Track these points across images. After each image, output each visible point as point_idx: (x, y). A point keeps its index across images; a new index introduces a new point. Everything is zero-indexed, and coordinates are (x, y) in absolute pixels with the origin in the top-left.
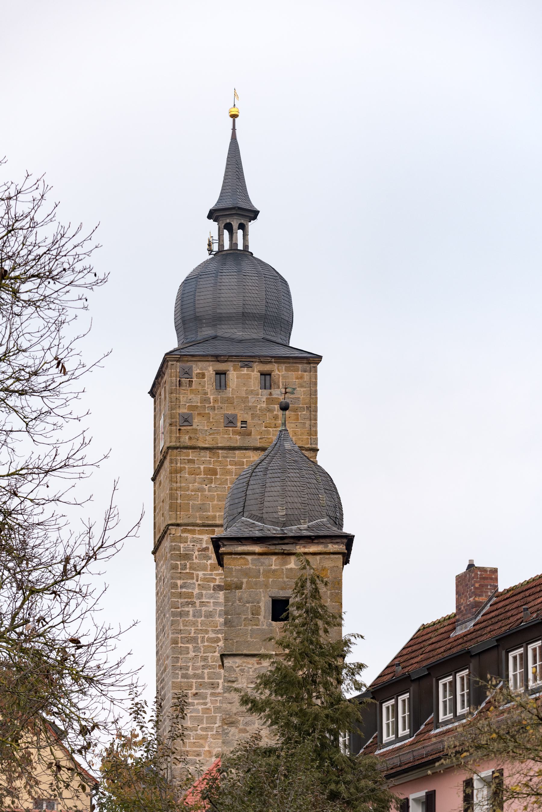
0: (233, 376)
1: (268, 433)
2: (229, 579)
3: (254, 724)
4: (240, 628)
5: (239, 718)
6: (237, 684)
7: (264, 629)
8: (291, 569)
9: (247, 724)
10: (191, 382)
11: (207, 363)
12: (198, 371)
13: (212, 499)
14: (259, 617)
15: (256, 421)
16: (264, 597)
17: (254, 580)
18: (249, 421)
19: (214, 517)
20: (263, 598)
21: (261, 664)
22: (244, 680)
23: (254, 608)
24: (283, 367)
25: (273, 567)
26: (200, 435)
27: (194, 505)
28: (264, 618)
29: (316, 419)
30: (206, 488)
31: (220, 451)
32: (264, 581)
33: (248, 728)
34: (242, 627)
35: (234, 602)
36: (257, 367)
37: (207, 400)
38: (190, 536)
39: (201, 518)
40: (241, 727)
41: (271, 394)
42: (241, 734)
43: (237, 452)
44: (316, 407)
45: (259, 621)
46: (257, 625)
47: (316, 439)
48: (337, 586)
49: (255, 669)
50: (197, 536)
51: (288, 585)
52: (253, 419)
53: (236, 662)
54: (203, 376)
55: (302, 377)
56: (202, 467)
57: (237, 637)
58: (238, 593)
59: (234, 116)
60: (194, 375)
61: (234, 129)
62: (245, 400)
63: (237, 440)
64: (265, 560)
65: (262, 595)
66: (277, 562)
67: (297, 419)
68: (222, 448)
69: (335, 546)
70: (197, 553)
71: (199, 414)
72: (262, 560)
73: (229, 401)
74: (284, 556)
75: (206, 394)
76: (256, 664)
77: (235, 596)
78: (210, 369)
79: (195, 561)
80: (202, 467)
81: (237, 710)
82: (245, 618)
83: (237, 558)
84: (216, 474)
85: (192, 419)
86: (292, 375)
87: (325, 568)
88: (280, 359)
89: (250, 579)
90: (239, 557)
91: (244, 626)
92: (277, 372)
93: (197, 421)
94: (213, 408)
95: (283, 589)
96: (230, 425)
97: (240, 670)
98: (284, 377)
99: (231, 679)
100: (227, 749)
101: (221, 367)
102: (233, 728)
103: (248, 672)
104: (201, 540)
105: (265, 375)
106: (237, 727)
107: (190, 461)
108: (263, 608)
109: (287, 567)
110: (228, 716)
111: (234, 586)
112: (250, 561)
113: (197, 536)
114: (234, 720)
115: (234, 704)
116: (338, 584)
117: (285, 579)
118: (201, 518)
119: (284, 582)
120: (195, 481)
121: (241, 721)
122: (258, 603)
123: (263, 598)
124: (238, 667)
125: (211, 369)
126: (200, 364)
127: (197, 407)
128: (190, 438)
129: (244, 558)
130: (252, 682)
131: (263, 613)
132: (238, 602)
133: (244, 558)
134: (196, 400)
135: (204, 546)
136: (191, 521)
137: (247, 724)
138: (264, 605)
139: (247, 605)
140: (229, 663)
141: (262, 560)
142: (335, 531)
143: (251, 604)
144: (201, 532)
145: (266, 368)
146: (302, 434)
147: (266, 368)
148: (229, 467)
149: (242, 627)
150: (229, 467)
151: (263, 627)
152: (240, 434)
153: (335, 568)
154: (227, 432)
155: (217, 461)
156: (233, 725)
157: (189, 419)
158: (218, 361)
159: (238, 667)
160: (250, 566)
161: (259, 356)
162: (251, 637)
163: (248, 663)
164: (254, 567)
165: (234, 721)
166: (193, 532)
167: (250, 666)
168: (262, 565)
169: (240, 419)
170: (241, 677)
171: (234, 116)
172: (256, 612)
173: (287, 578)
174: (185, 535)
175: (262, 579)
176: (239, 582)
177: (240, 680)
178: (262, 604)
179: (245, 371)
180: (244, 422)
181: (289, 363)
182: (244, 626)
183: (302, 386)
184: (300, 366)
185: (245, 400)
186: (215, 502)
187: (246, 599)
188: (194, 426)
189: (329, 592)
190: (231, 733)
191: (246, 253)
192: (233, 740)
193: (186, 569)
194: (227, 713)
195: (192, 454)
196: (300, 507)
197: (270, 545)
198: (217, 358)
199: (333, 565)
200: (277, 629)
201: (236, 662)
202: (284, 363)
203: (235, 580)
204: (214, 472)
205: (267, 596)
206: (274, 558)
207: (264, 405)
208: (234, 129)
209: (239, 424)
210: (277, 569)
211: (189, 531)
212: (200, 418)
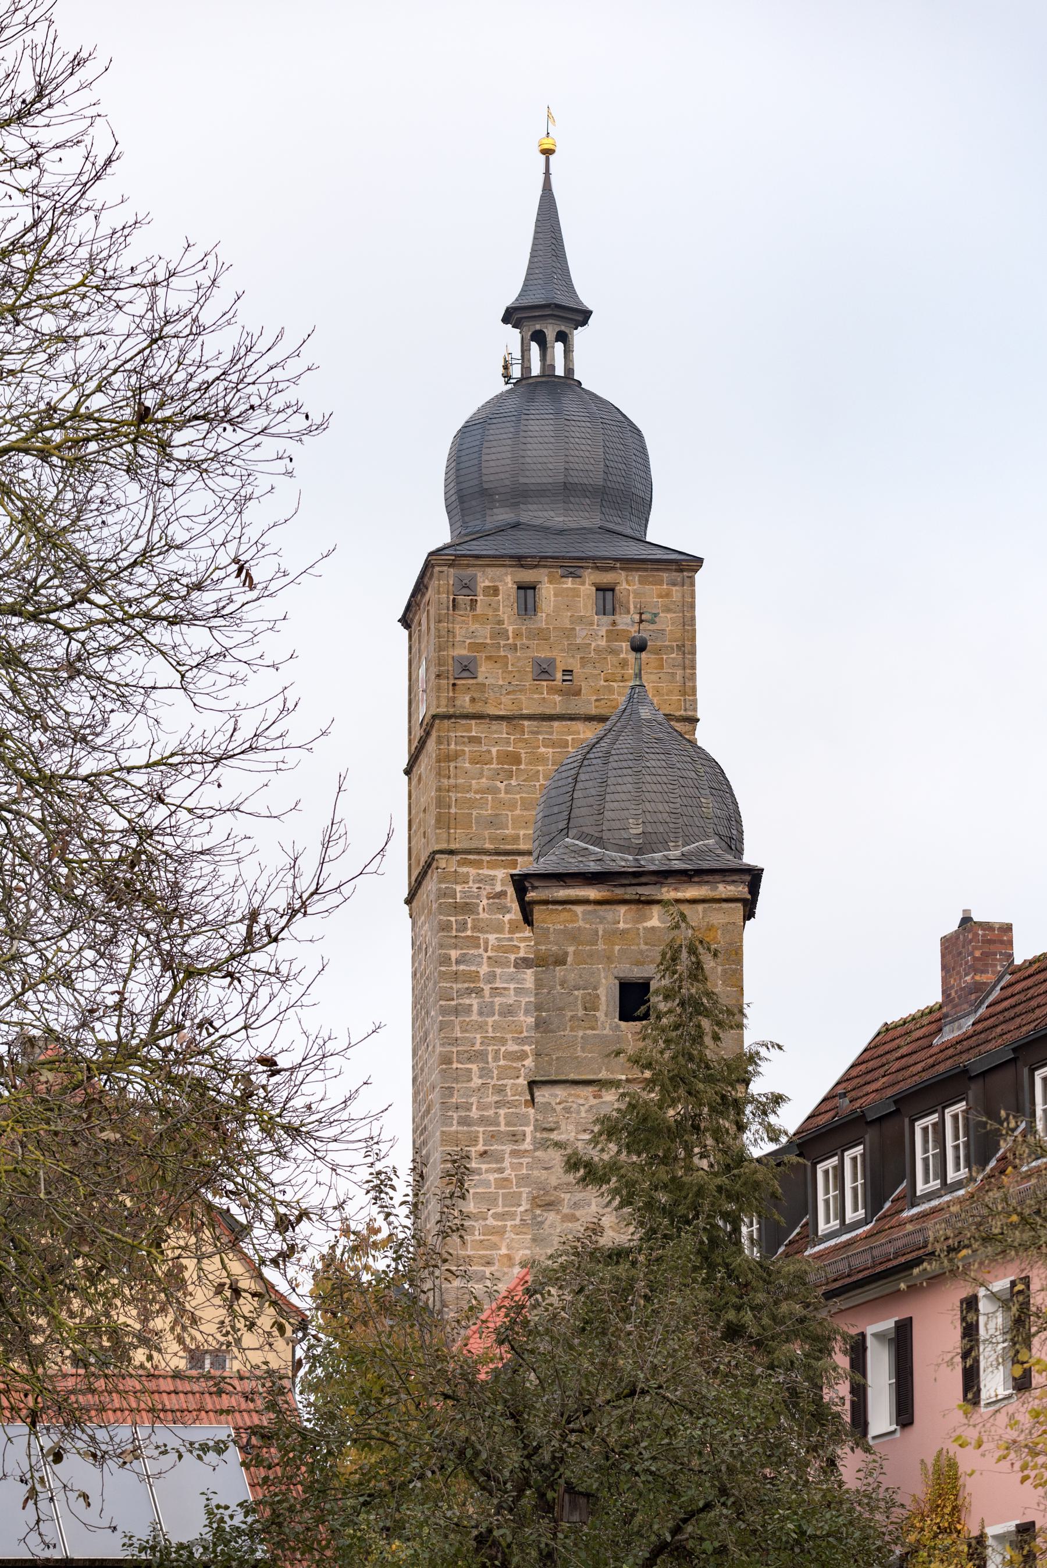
0: (548, 592)
2: (544, 948)
3: (589, 1205)
5: (562, 1195)
6: (559, 1134)
7: (606, 1036)
8: (653, 928)
9: (576, 1205)
10: (474, 602)
11: (503, 570)
12: (487, 583)
13: (512, 806)
15: (588, 670)
16: (606, 978)
17: (588, 948)
18: (577, 669)
19: (516, 839)
20: (603, 981)
21: (600, 1097)
22: (571, 1127)
23: (588, 998)
24: (636, 576)
25: (621, 925)
26: (490, 695)
27: (480, 816)
28: (606, 1016)
30: (502, 786)
31: (526, 723)
33: (578, 1213)
34: (566, 1033)
36: (591, 577)
38: (472, 871)
39: (492, 840)
40: (566, 1210)
41: (614, 623)
42: (565, 1225)
43: (556, 724)
44: (694, 646)
46: (593, 1029)
47: (695, 701)
50: (486, 872)
51: (647, 956)
52: (583, 666)
53: (557, 1095)
54: (496, 591)
55: (668, 595)
56: (494, 750)
59: (547, 152)
60: (479, 590)
61: (547, 173)
62: (570, 633)
63: (557, 704)
64: (608, 913)
65: (602, 975)
67: (661, 667)
69: (729, 888)
70: (485, 902)
71: (489, 658)
73: (541, 635)
75: (500, 622)
76: (591, 1098)
77: (554, 977)
78: (507, 580)
79: (483, 915)
80: (494, 750)
84: (519, 763)
85: (476, 666)
88: (630, 564)
90: (560, 908)
93: (485, 671)
95: (638, 963)
96: (545, 676)
98: (637, 594)
100: (541, 1252)
103: (579, 1112)
104: (493, 878)
106: (558, 1212)
108: (603, 999)
109: (645, 924)
110: (542, 1192)
111: (551, 960)
113: (486, 872)
114: (552, 1198)
116: (737, 954)
117: (643, 947)
118: (492, 840)
119: (641, 952)
120: (481, 775)
122: (595, 988)
123: (603, 981)
124: (560, 1103)
125: (509, 579)
126: (490, 571)
127: (484, 645)
128: (473, 700)
129: (570, 910)
130: (585, 1131)
131: (603, 1007)
132: (559, 987)
133: (570, 910)
134: (484, 633)
136: (474, 844)
137: (576, 1205)
139: (576, 993)
140: (544, 1096)
144: (492, 865)
146: (670, 692)
147: (607, 578)
148: (542, 750)
149: (566, 1033)
150: (542, 750)
151: (605, 1032)
152: (560, 692)
154: (537, 690)
155: (521, 740)
156: (551, 1208)
157: (471, 667)
158: (522, 566)
159: (560, 1103)
160: (581, 923)
161: (594, 558)
162: (583, 1049)
163: (578, 1096)
164: (588, 926)
166: (478, 864)
167: (581, 1101)
168: (601, 923)
170: (565, 1121)
171: (547, 152)
172: (590, 1005)
173: (646, 944)
174: (464, 870)
175: (601, 946)
177: (563, 1127)
178: (602, 992)
179: (569, 583)
180: (568, 672)
181: (646, 570)
183: (668, 610)
184: (665, 575)
185: (570, 633)
186: (518, 812)
187: (573, 983)
188: (480, 679)
189: (720, 968)
190: (548, 1222)
193: (465, 929)
195: (475, 729)
197: (615, 886)
198: (520, 561)
200: (630, 1036)
201: (557, 1095)
202: (638, 570)
204: (516, 759)
205: (611, 977)
207: (603, 643)
208: (547, 173)
209: (559, 676)
210: (628, 929)
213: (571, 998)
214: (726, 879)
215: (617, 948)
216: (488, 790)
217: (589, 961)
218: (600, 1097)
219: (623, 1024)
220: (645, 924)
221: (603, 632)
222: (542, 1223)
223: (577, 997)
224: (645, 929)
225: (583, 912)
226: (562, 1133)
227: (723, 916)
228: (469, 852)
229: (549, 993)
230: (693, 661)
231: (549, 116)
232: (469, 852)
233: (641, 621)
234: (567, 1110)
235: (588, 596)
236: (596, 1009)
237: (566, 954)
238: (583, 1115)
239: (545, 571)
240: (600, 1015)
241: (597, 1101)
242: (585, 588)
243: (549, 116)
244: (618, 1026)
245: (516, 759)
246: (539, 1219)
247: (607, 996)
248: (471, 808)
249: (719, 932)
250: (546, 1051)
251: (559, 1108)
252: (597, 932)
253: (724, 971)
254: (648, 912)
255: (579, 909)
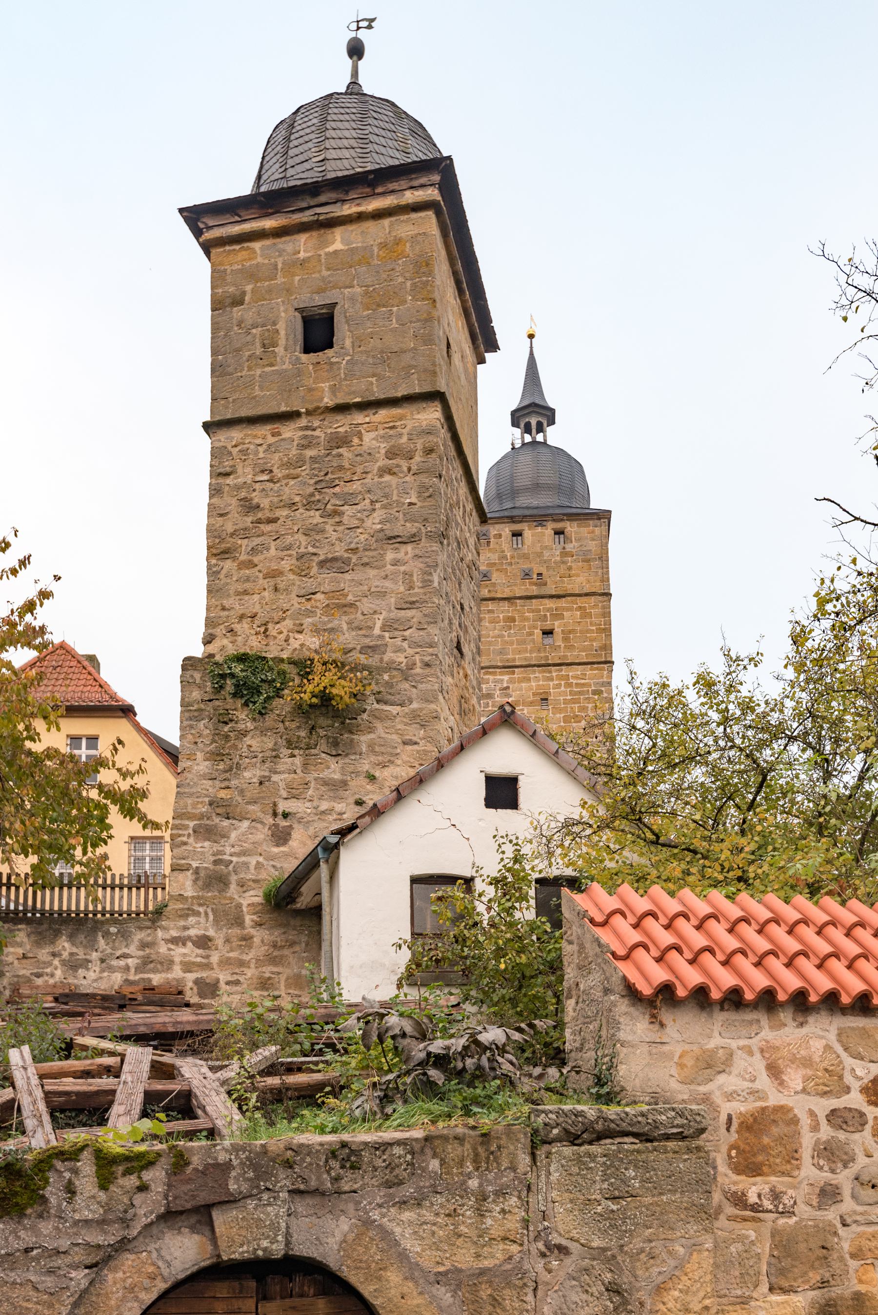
0: (528, 534)
1: (563, 582)
2: (220, 291)
3: (268, 549)
4: (239, 374)
5: (239, 542)
6: (236, 478)
7: (286, 371)
8: (336, 252)
9: (254, 551)
10: (489, 543)
11: (504, 525)
12: (496, 532)
13: (512, 643)
14: (276, 350)
15: (551, 572)
16: (285, 311)
17: (267, 283)
18: (544, 572)
19: (514, 660)
20: (283, 314)
21: (279, 434)
22: (248, 470)
23: (267, 334)
24: (575, 524)
25: (302, 255)
26: (498, 588)
27: (494, 649)
28: (286, 350)
29: (608, 568)
30: (506, 634)
31: (518, 601)
32: (284, 283)
33: (256, 560)
34: (244, 373)
35: (229, 330)
36: (551, 526)
37: (505, 557)
38: (491, 677)
39: (501, 661)
40: (243, 557)
41: (564, 548)
42: (242, 572)
43: (534, 601)
44: (608, 557)
45: (275, 357)
46: (272, 365)
47: (609, 585)
48: (424, 269)
49: (270, 445)
50: (498, 677)
51: (330, 282)
52: (548, 571)
53: (233, 438)
54: (500, 536)
55: (593, 532)
56: (501, 616)
57: (235, 391)
58: (237, 312)
59: (531, 336)
60: (492, 536)
61: (531, 347)
62: (540, 555)
63: (534, 590)
64: (287, 244)
65: (282, 309)
66: (309, 245)
67: (590, 569)
68: (520, 598)
69: (416, 193)
70: (498, 692)
71: (497, 570)
72: (281, 246)
73: (526, 557)
74: (322, 231)
75: (503, 551)
76: (269, 436)
77: (231, 318)
78: (506, 530)
79: (497, 699)
80: (501, 616)
81: (235, 527)
82: (250, 356)
83: (234, 250)
84: (515, 621)
85: (491, 574)
86: (584, 531)
87: (400, 239)
88: (572, 517)
89: (259, 284)
90: (237, 247)
91: (248, 370)
92: (569, 529)
93: (496, 577)
94: (511, 564)
95: (320, 291)
96: (527, 577)
97: (240, 451)
98: (576, 533)
99: (222, 470)
100: (216, 603)
101: (517, 527)
102: (229, 562)
103: (256, 453)
104: (502, 680)
105: (559, 532)
106: (234, 559)
107: (490, 611)
108: (282, 333)
109: (327, 250)
110: (217, 541)
111: (228, 301)
112: (258, 252)
113: (498, 677)
114: (228, 545)
115: (229, 516)
116: (427, 265)
117: (325, 273)
118: (501, 661)
119: (323, 279)
120: (495, 629)
121: (244, 547)
122: (274, 323)
123: (283, 314)
124: (236, 446)
125: (507, 530)
126: (497, 526)
127: (495, 564)
128: (489, 591)
129: (248, 248)
130: (263, 471)
131: (282, 342)
132: (236, 328)
133: (248, 248)
134: (494, 557)
135: (505, 685)
136: (493, 663)
137: (254, 551)
138: (284, 326)
139: (254, 331)
140: (220, 441)
141: (281, 246)
142: (418, 154)
143: (260, 329)
144: (501, 674)
145: (559, 525)
146: (595, 581)
147: (559, 525)
148: (527, 614)
149: (244, 373)
150: (527, 614)
151: (284, 367)
152: (536, 584)
153: (420, 238)
154: (524, 584)
155: (516, 610)
156: (227, 556)
157: (488, 575)
158: (514, 522)
159: (236, 446)
160: (259, 259)
161: (551, 515)
162: (261, 388)
163: (255, 436)
164: (266, 261)
165: (229, 548)
166: (494, 674)
167: (259, 441)
168: (280, 256)
169: (536, 571)
170: (241, 464)
171: (531, 336)
172: (269, 344)
173: (328, 269)
174: (487, 677)
175: (280, 280)
176: (238, 293)
177: (240, 470)
178: (281, 326)
179: (539, 529)
180: (540, 574)
181: (580, 520)
182: (248, 370)
183: (593, 540)
184: (591, 522)
185: (540, 555)
186: (515, 646)
187: (250, 321)
188: (493, 581)
189: (409, 283)
190: (224, 572)
191: (545, 443)
192: (227, 584)
193: (488, 707)
194: (216, 534)
195: (491, 606)
196: (355, 145)
197: (293, 212)
198: (512, 519)
199: (416, 232)
200: (311, 367)
201: (233, 438)
202: (576, 520)
203: (232, 289)
204: (513, 620)
205: (291, 312)
206: (303, 238)
207: (558, 558)
208: (531, 347)
209: (535, 576)
210: (309, 258)
211: (490, 673)
212: (498, 573)
213: (249, 338)
214: (416, 183)
215: (297, 278)
216: (499, 636)
217: (267, 297)
218: (279, 434)
219: (304, 357)
220: (327, 250)
221: (558, 553)
222: (219, 572)
223: (254, 336)
224: (326, 254)
225: (261, 248)
226: (238, 477)
227: (412, 227)
228: (489, 667)
229: (225, 335)
230: (608, 564)
231: (532, 319)
232: (489, 667)
233: (358, 28)
234: (245, 452)
235: (550, 535)
236: (275, 345)
237: (244, 293)
238: (261, 455)
239: (526, 524)
240: (280, 350)
241: (276, 439)
242: (548, 530)
243: (532, 319)
244: (298, 359)
245: (513, 620)
246: (215, 569)
247: (286, 330)
248: (490, 645)
249: (408, 245)
250: (222, 395)
251: (235, 451)
252: (276, 265)
253: (414, 285)
254: (330, 237)
255: (257, 245)
